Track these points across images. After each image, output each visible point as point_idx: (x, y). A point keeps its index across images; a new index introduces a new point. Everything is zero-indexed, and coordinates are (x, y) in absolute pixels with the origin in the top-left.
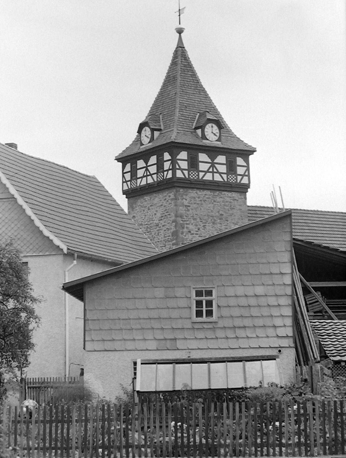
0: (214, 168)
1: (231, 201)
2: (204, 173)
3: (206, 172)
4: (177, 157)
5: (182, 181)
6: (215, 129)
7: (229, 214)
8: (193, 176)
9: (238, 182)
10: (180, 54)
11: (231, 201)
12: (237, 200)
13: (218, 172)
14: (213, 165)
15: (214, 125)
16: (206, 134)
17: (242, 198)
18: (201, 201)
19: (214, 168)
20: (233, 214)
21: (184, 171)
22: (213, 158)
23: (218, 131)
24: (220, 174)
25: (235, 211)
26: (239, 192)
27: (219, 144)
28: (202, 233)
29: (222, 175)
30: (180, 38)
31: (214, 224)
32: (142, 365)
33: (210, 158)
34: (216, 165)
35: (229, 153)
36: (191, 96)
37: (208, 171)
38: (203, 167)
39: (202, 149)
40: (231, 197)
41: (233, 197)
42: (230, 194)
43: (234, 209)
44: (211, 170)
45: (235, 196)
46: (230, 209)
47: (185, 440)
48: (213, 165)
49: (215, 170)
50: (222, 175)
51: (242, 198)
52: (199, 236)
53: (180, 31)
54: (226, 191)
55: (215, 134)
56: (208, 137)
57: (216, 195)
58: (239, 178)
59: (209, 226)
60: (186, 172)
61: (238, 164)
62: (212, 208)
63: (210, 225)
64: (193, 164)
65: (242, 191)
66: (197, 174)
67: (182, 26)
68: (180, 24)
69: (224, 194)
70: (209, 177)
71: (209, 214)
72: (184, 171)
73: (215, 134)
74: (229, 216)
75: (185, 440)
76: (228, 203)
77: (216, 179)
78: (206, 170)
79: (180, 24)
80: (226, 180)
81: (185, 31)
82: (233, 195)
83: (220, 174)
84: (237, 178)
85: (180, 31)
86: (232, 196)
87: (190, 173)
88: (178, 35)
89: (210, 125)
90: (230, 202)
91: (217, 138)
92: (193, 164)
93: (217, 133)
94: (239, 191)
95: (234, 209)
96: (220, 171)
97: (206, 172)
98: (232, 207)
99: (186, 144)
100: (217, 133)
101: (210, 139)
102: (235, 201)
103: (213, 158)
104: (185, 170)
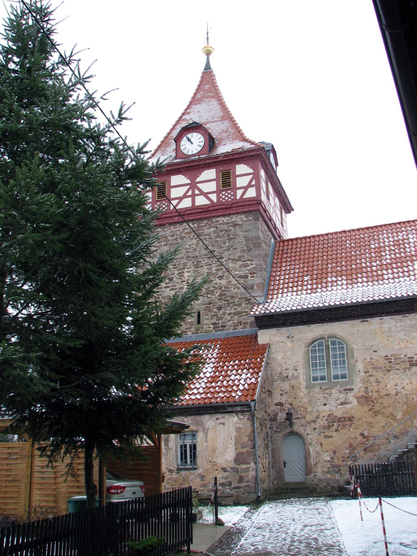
1: (230, 228)
3: (246, 188)
8: (227, 196)
10: (208, 74)
14: (193, 186)
15: (189, 136)
18: (176, 239)
28: (176, 284)
29: (243, 190)
30: (208, 59)
31: (197, 267)
38: (241, 182)
47: (408, 486)
48: (193, 186)
49: (197, 192)
52: (171, 290)
53: (208, 53)
54: (219, 216)
57: (202, 226)
59: (188, 272)
62: (194, 246)
63: (191, 270)
64: (226, 181)
65: (208, 215)
69: (216, 221)
70: (186, 203)
71: (189, 254)
75: (408, 486)
77: (197, 204)
83: (206, 195)
85: (208, 53)
90: (226, 231)
96: (205, 191)
98: (231, 236)
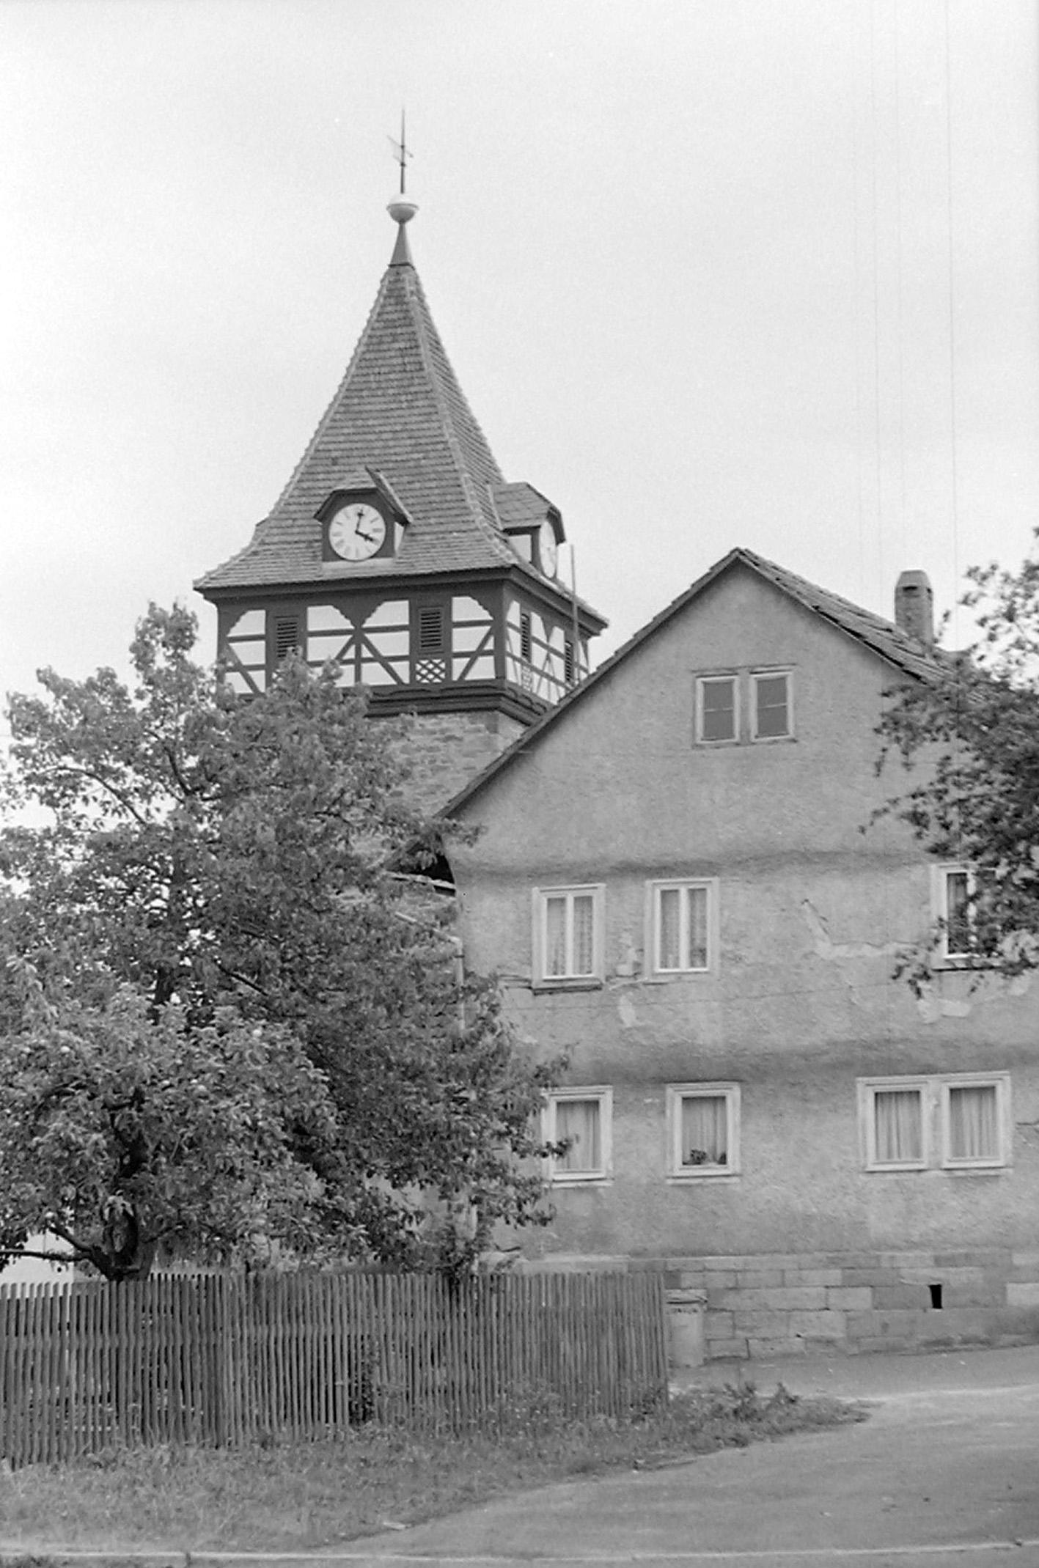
0: (364, 648)
2: (467, 660)
3: (473, 656)
4: (364, 622)
5: (477, 692)
6: (373, 520)
7: (424, 789)
9: (455, 677)
11: (436, 743)
12: (460, 739)
13: (377, 657)
16: (334, 540)
17: (479, 731)
19: (364, 648)
20: (439, 787)
21: (252, 674)
22: (357, 617)
23: (380, 524)
24: (385, 662)
25: (449, 776)
26: (468, 711)
27: (384, 566)
29: (392, 664)
32: (943, 1304)
33: (485, 608)
34: (368, 635)
35: (415, 588)
36: (370, 423)
37: (481, 652)
38: (464, 640)
39: (311, 594)
40: (434, 733)
41: (442, 731)
42: (430, 723)
43: (445, 768)
44: (351, 654)
45: (451, 726)
46: (429, 773)
48: (358, 637)
49: (366, 653)
50: (392, 664)
51: (479, 731)
53: (402, 215)
55: (366, 537)
56: (340, 552)
58: (459, 665)
60: (259, 677)
61: (456, 617)
64: (430, 634)
66: (443, 666)
67: (404, 199)
68: (402, 191)
72: (252, 674)
73: (366, 537)
74: (424, 794)
76: (423, 752)
78: (473, 648)
79: (402, 191)
80: (406, 680)
81: (418, 214)
82: (445, 725)
83: (385, 662)
84: (449, 666)
85: (402, 215)
86: (437, 728)
87: (419, 667)
88: (397, 225)
89: (351, 510)
90: (431, 749)
91: (374, 548)
92: (430, 634)
93: (375, 530)
94: (451, 707)
95: (445, 768)
96: (385, 653)
97: (473, 656)
98: (439, 763)
99: (251, 587)
100: (375, 530)
101: (352, 556)
102: (452, 744)
103: (357, 617)
104: (557, 653)
